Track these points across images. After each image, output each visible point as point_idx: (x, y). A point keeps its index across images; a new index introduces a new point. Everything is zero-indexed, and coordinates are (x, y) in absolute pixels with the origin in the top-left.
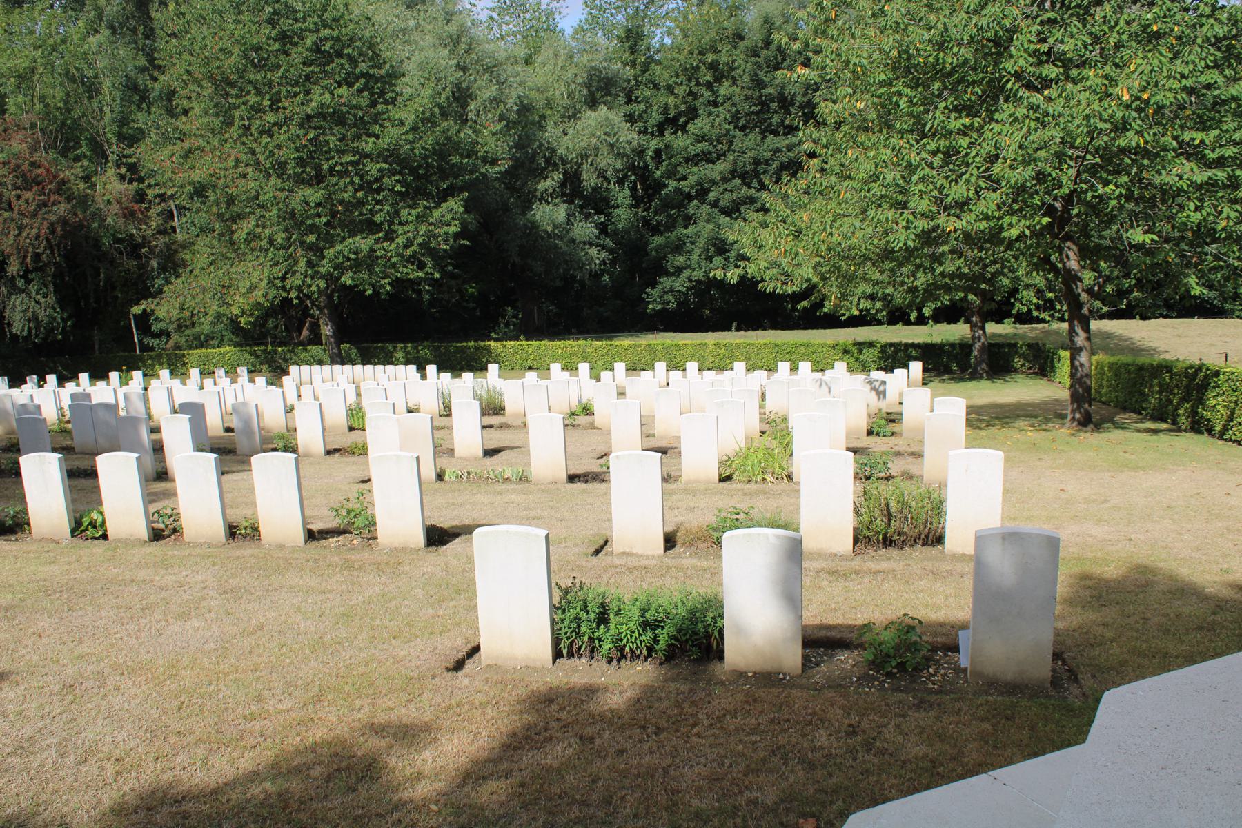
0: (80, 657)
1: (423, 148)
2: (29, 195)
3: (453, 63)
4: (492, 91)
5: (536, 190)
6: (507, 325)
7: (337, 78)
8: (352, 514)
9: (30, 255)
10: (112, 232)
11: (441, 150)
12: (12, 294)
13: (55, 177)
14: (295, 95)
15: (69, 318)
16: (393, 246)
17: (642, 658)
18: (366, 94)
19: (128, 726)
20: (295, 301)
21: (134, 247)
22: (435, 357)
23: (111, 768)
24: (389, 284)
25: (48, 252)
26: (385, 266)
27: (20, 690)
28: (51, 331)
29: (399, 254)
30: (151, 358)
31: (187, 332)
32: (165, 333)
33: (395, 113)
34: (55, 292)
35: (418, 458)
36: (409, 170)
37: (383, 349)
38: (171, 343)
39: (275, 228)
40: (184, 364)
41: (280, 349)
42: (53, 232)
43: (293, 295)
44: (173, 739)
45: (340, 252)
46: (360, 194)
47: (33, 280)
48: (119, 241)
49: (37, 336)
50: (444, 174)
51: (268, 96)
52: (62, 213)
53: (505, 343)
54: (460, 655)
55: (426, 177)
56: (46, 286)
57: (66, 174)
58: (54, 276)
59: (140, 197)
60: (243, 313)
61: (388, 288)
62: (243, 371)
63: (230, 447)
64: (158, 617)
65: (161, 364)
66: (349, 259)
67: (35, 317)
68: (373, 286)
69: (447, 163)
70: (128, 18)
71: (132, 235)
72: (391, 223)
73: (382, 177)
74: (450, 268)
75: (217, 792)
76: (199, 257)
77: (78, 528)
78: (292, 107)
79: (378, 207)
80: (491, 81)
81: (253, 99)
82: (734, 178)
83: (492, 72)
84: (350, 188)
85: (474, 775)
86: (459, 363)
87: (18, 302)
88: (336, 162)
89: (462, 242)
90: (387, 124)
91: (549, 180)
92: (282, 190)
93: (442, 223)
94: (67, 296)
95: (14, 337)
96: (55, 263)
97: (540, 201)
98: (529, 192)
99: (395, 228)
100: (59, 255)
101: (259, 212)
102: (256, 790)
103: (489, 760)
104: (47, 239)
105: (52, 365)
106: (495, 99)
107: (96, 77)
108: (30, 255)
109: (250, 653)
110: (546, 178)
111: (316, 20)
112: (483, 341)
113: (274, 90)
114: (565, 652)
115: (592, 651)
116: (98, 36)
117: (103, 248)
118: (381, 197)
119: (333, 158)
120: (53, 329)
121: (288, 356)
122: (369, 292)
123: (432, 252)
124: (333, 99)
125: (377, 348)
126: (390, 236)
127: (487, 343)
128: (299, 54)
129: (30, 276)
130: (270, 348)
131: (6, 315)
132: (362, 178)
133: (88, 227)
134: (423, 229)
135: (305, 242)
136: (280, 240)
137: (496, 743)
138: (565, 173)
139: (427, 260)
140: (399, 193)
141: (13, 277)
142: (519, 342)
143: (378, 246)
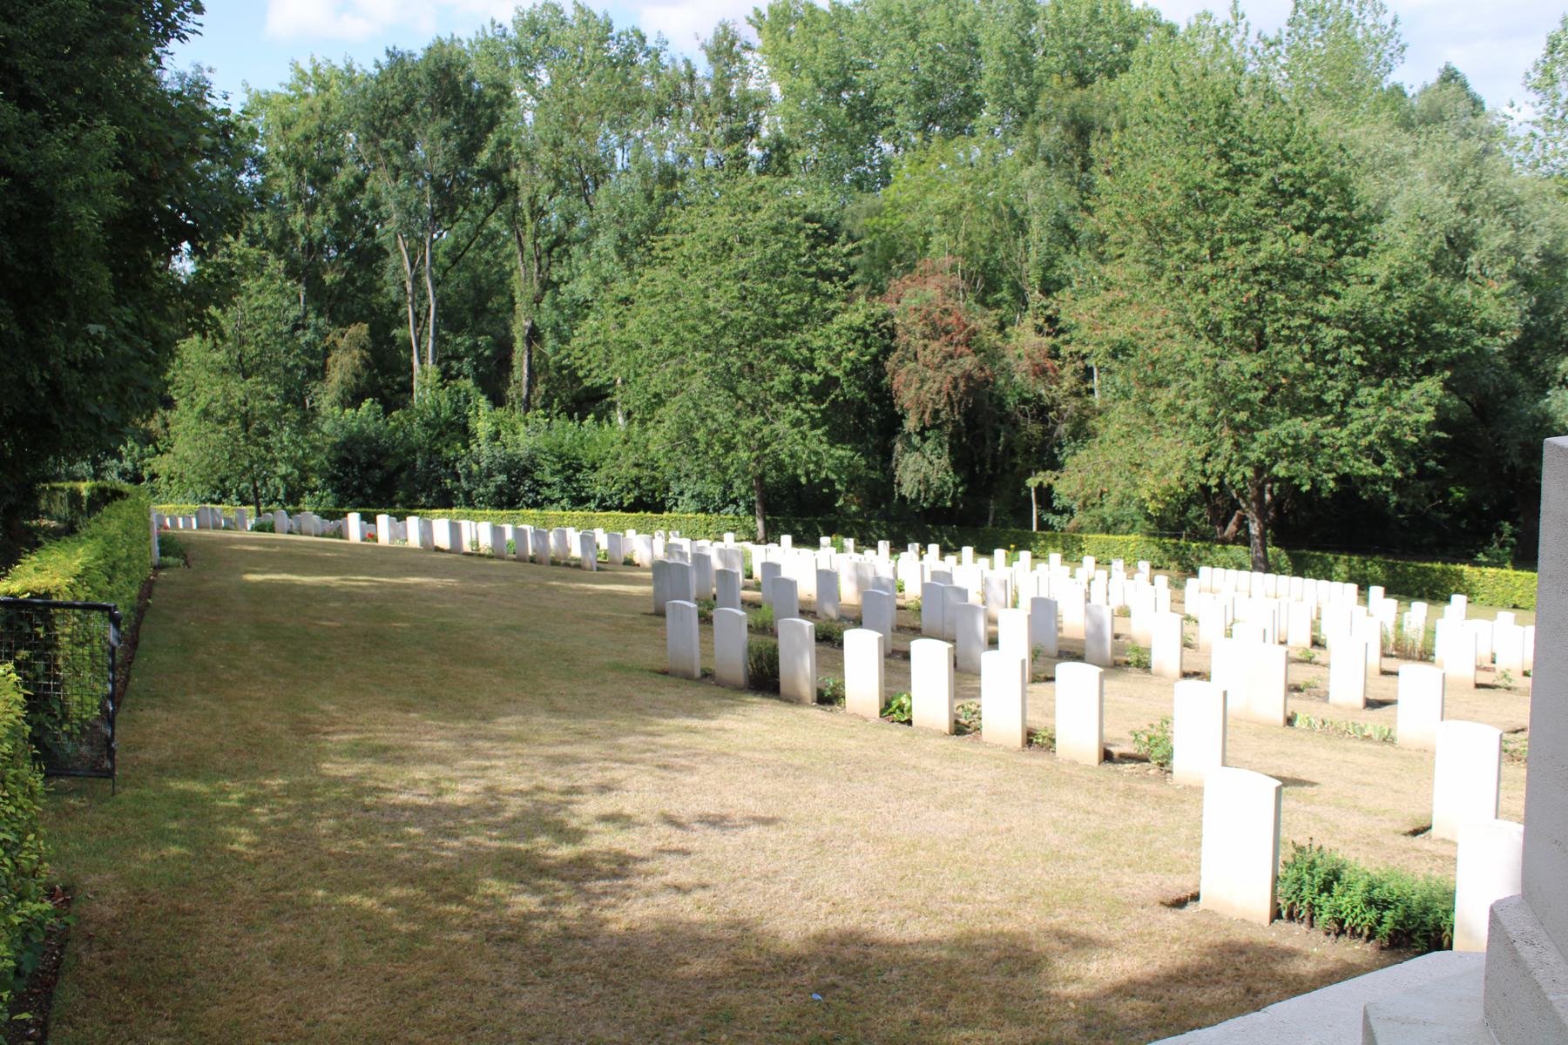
0: (840, 820)
1: (1396, 312)
2: (935, 345)
3: (1453, 201)
4: (1507, 236)
5: (1556, 370)
6: (1502, 546)
7: (1296, 222)
8: (1153, 742)
9: (928, 411)
11: (1423, 315)
13: (966, 326)
14: (1241, 242)
15: (961, 483)
16: (1345, 433)
17: (1364, 938)
18: (1330, 242)
19: (854, 882)
20: (1214, 490)
21: (1041, 411)
22: (1388, 577)
23: (826, 907)
24: (1334, 479)
25: (948, 409)
26: (1331, 457)
27: (782, 835)
28: (940, 496)
29: (1351, 444)
30: (1045, 538)
31: (1093, 511)
32: (1067, 511)
33: (1365, 268)
35: (1225, 693)
36: (1377, 339)
37: (1321, 559)
38: (1073, 523)
39: (1199, 400)
40: (1081, 550)
41: (1194, 545)
42: (955, 387)
43: (1213, 482)
44: (885, 900)
45: (1276, 436)
46: (1309, 366)
47: (929, 438)
48: (1025, 401)
49: (926, 500)
50: (1423, 344)
51: (1207, 244)
52: (967, 367)
54: (1183, 895)
55: (1399, 347)
56: (941, 446)
57: (980, 323)
58: (951, 436)
59: (1054, 353)
60: (1154, 497)
61: (1332, 484)
62: (1144, 566)
63: (1079, 652)
64: (920, 801)
65: (1055, 547)
66: (1285, 445)
67: (926, 480)
68: (1313, 480)
69: (1429, 331)
70: (1065, 148)
71: (1040, 396)
72: (1344, 403)
73: (1339, 347)
74: (1431, 463)
75: (900, 946)
76: (1111, 428)
77: (886, 708)
78: (1237, 257)
79: (1330, 383)
80: (1504, 225)
81: (1190, 246)
82: (727, 506)
83: (1507, 213)
84: (1298, 358)
85: (1126, 990)
86: (1419, 588)
87: (911, 461)
88: (1283, 326)
90: (1352, 280)
92: (1213, 356)
94: (962, 460)
95: (903, 498)
97: (1560, 384)
98: (1546, 373)
99: (1349, 410)
101: (1184, 380)
102: (932, 954)
103: (1148, 984)
104: (949, 394)
107: (1025, 213)
108: (928, 411)
109: (987, 849)
111: (1277, 153)
112: (1454, 563)
113: (1217, 237)
114: (1284, 913)
115: (1311, 919)
116: (1032, 168)
117: (1008, 409)
119: (1278, 320)
120: (942, 495)
121: (1202, 555)
122: (1306, 488)
123: (1396, 444)
124: (1287, 247)
125: (1313, 557)
126: (1341, 419)
127: (1459, 567)
128: (1254, 190)
129: (927, 434)
130: (1182, 542)
131: (897, 473)
132: (1314, 344)
133: (994, 383)
134: (1386, 414)
135: (1233, 420)
136: (1204, 416)
137: (1162, 973)
139: (1388, 454)
140: (1360, 367)
142: (1504, 571)
143: (1325, 431)
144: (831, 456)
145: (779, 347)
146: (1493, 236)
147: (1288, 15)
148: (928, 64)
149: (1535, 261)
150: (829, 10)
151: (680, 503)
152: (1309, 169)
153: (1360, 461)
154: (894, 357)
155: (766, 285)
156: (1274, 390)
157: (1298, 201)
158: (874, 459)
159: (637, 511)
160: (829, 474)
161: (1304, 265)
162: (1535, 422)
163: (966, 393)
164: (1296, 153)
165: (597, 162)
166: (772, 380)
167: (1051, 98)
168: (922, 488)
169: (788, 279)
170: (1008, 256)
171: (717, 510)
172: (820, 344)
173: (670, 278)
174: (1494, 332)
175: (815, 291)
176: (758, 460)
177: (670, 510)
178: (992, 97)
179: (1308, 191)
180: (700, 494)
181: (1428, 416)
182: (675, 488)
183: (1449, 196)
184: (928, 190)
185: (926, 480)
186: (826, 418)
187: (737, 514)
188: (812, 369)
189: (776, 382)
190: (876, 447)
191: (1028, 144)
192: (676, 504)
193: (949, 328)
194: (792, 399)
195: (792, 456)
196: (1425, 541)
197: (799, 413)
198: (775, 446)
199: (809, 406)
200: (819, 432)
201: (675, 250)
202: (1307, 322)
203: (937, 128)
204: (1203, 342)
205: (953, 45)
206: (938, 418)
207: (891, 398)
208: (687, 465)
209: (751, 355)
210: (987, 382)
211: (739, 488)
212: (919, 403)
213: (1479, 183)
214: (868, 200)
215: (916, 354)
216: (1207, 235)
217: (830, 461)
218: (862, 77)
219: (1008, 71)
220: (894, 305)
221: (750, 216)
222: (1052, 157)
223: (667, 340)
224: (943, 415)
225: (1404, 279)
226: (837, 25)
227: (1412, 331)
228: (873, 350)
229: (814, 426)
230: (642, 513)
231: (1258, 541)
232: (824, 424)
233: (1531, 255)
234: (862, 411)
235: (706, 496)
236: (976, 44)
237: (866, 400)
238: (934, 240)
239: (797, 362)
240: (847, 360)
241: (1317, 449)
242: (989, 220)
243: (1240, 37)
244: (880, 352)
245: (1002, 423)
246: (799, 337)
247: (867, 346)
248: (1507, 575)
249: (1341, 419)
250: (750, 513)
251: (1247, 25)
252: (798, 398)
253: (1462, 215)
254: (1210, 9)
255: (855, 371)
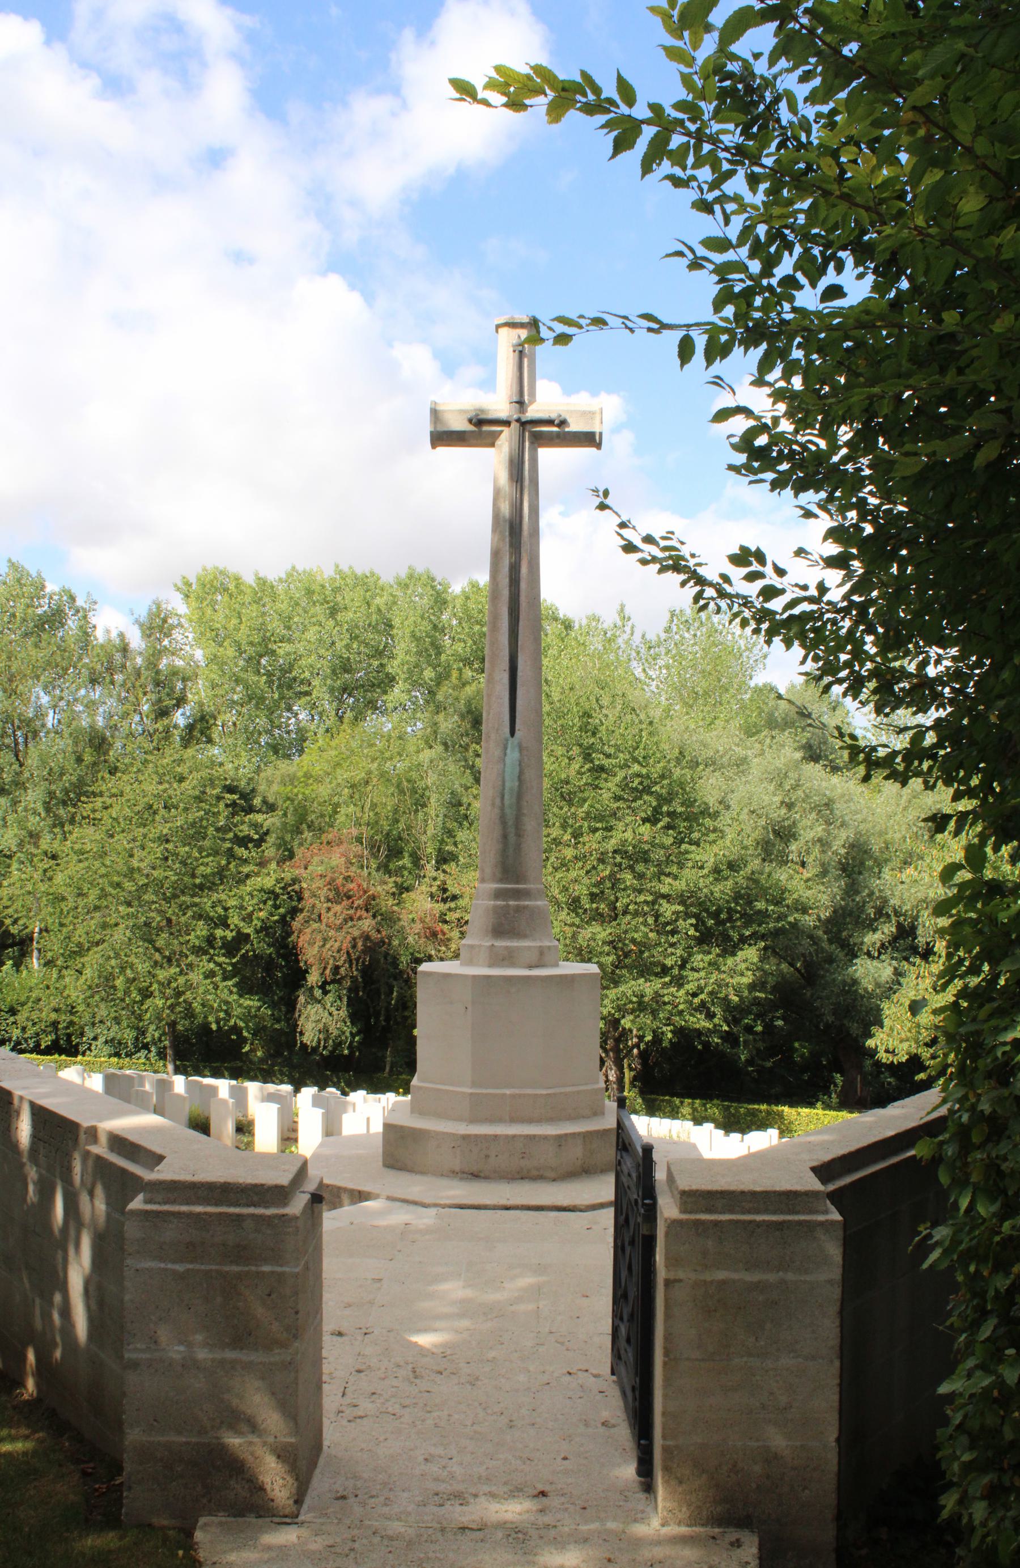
2: (338, 908)
3: (777, 799)
4: (819, 830)
5: (862, 943)
9: (329, 967)
10: (411, 951)
12: (308, 1003)
14: (596, 830)
15: (358, 1033)
16: (682, 992)
24: (671, 1031)
25: (347, 965)
28: (338, 1045)
29: (686, 1002)
33: (697, 854)
34: (348, 1005)
35: (368, 1119)
37: (669, 1102)
42: (354, 947)
47: (330, 991)
49: (325, 1047)
50: (749, 919)
51: (569, 830)
52: (366, 929)
53: (800, 1110)
56: (340, 999)
58: (350, 990)
61: (670, 1035)
66: (631, 1002)
67: (326, 1030)
68: (654, 1032)
72: (682, 967)
73: (676, 920)
78: (591, 842)
79: (670, 950)
82: (139, 1051)
83: (820, 811)
89: (758, 994)
91: (880, 932)
92: (573, 925)
93: (733, 972)
95: (304, 1046)
96: (351, 977)
100: (357, 970)
104: (348, 953)
105: (335, 1080)
106: (820, 840)
108: (329, 967)
110: (875, 930)
118: (675, 940)
120: (340, 1043)
125: (663, 1101)
126: (679, 982)
127: (780, 1108)
128: (611, 785)
129: (328, 988)
131: (300, 1023)
138: (899, 926)
141: (312, 987)
142: (815, 1111)
143: (665, 991)
144: (240, 1006)
145: (196, 905)
146: (810, 829)
147: (664, 624)
148: (344, 642)
149: (843, 851)
150: (254, 585)
151: (93, 1048)
152: (656, 771)
153: (694, 1016)
154: (300, 917)
155: (187, 849)
156: (626, 955)
157: (646, 797)
158: (280, 1010)
159: (51, 1054)
160: (238, 1021)
161: (649, 850)
162: (844, 987)
163: (363, 952)
164: (644, 758)
165: (29, 722)
166: (189, 934)
167: (450, 691)
168: (321, 1036)
169: (207, 843)
170: (409, 828)
171: (129, 1055)
172: (234, 903)
173: (99, 838)
174: (805, 910)
175: (230, 854)
176: (172, 1007)
177: (84, 1054)
178: (403, 676)
179: (653, 789)
180: (113, 1040)
181: (747, 979)
182: (89, 1033)
183: (775, 795)
184: (338, 765)
185: (326, 1030)
186: (236, 971)
187: (148, 1059)
188: (227, 926)
189: (192, 937)
190: (281, 999)
191: (429, 729)
192: (89, 1049)
193: (351, 893)
194: (206, 953)
195: (203, 1005)
196: (773, 1091)
197: (212, 965)
198: (188, 995)
199: (222, 959)
200: (230, 983)
201: (105, 812)
202: (650, 898)
203: (352, 700)
204: (565, 913)
205: (369, 625)
206: (338, 973)
207: (297, 955)
208: (102, 1012)
209: (170, 911)
210: (384, 943)
211: (152, 1033)
212: (321, 960)
213: (798, 785)
214: (284, 767)
215: (320, 916)
216: (570, 821)
217: (239, 1010)
218: (283, 649)
219: (419, 653)
220: (302, 871)
221: (175, 785)
222: (450, 743)
223: (93, 894)
224: (342, 971)
225: (732, 866)
226: (261, 599)
227: (739, 908)
228: (282, 910)
229: (225, 979)
230: (56, 1056)
231: (615, 1086)
232: (234, 976)
233: (838, 846)
234: (269, 965)
235: (120, 1043)
236: (391, 626)
237: (273, 956)
238: (343, 810)
239: (212, 919)
240: (258, 919)
241: (660, 1006)
242: (393, 794)
243: (626, 636)
244: (288, 912)
245: (395, 979)
246: (215, 896)
247: (276, 907)
248: (817, 1114)
249: (679, 982)
250: (161, 1059)
251: (633, 627)
252: (212, 951)
253: (783, 811)
254: (598, 613)
255: (264, 929)
